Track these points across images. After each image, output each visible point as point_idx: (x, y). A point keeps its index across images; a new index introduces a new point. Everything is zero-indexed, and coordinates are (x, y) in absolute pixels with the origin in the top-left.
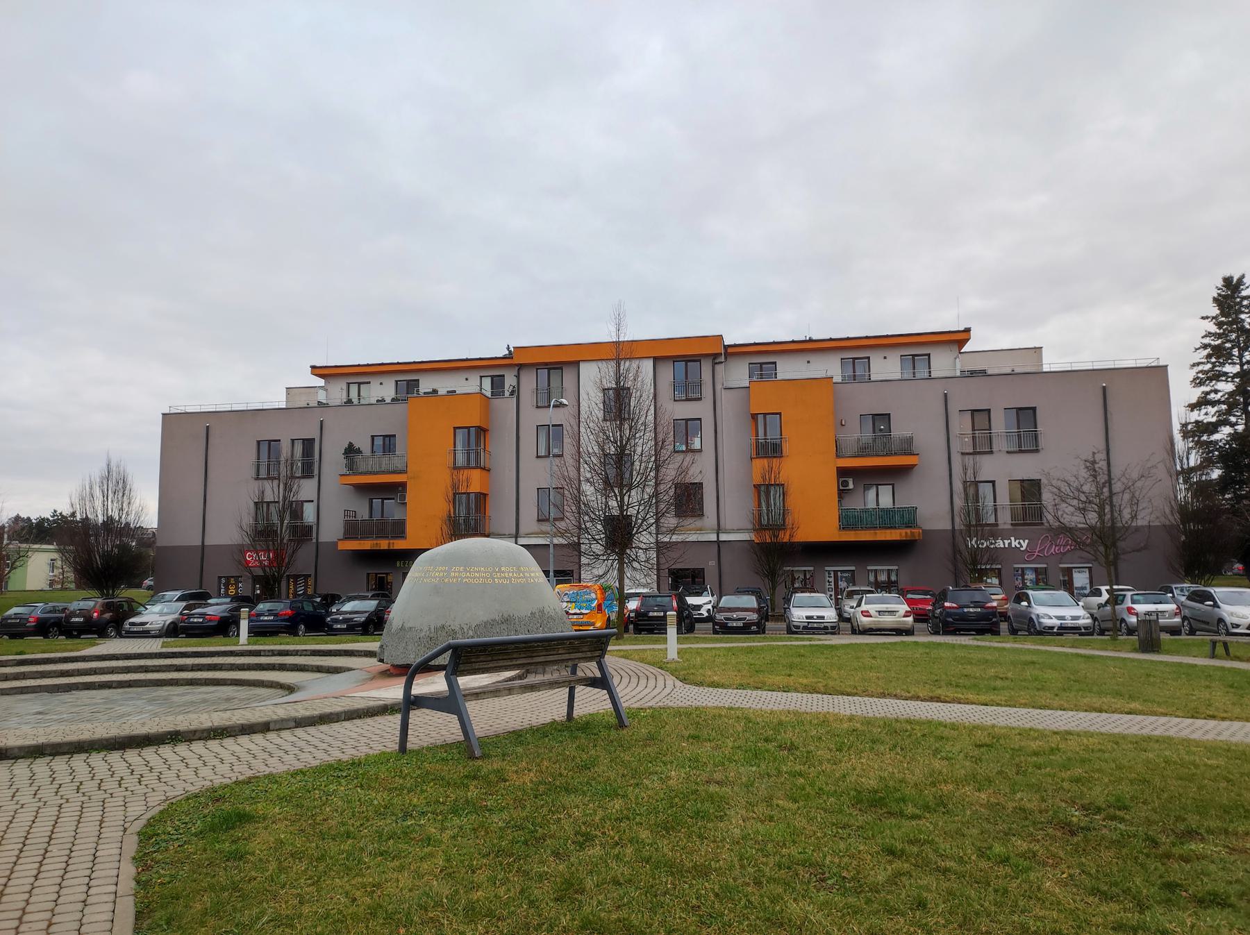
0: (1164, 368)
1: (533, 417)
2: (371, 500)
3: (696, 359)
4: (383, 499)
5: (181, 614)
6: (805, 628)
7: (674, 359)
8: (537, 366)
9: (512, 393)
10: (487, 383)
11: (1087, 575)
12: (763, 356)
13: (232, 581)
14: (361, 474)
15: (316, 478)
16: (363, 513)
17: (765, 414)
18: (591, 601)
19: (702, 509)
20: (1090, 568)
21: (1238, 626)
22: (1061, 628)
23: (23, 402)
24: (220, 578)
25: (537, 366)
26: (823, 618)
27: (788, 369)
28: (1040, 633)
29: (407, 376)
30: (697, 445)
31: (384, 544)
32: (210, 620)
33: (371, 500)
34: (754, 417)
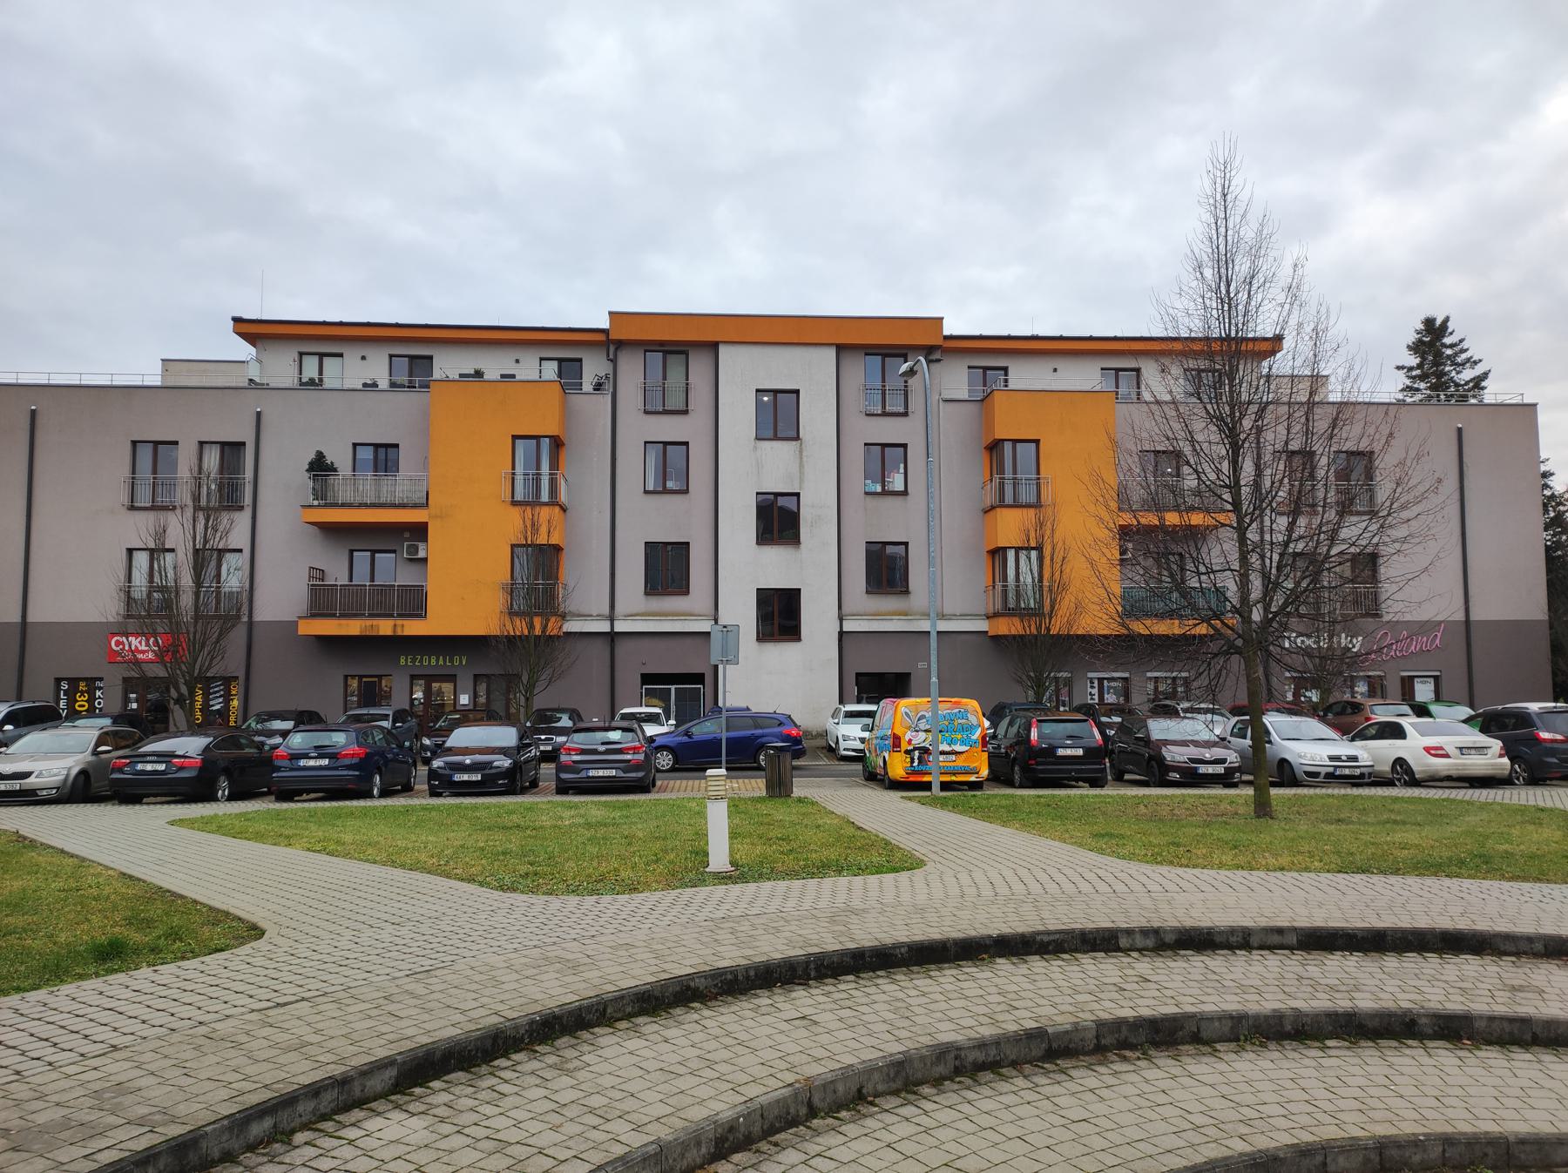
1: (639, 428)
2: (351, 552)
3: (902, 352)
4: (373, 552)
5: (95, 753)
6: (1329, 776)
7: (869, 350)
8: (648, 346)
9: (598, 387)
10: (550, 371)
11: (1431, 686)
12: (991, 355)
13: (82, 686)
14: (335, 505)
15: (247, 513)
16: (337, 575)
17: (1015, 441)
18: (971, 728)
20: (1436, 678)
24: (58, 681)
25: (648, 346)
26: (1355, 759)
27: (1025, 375)
30: (897, 482)
31: (385, 627)
32: (181, 768)
33: (351, 552)
34: (994, 447)
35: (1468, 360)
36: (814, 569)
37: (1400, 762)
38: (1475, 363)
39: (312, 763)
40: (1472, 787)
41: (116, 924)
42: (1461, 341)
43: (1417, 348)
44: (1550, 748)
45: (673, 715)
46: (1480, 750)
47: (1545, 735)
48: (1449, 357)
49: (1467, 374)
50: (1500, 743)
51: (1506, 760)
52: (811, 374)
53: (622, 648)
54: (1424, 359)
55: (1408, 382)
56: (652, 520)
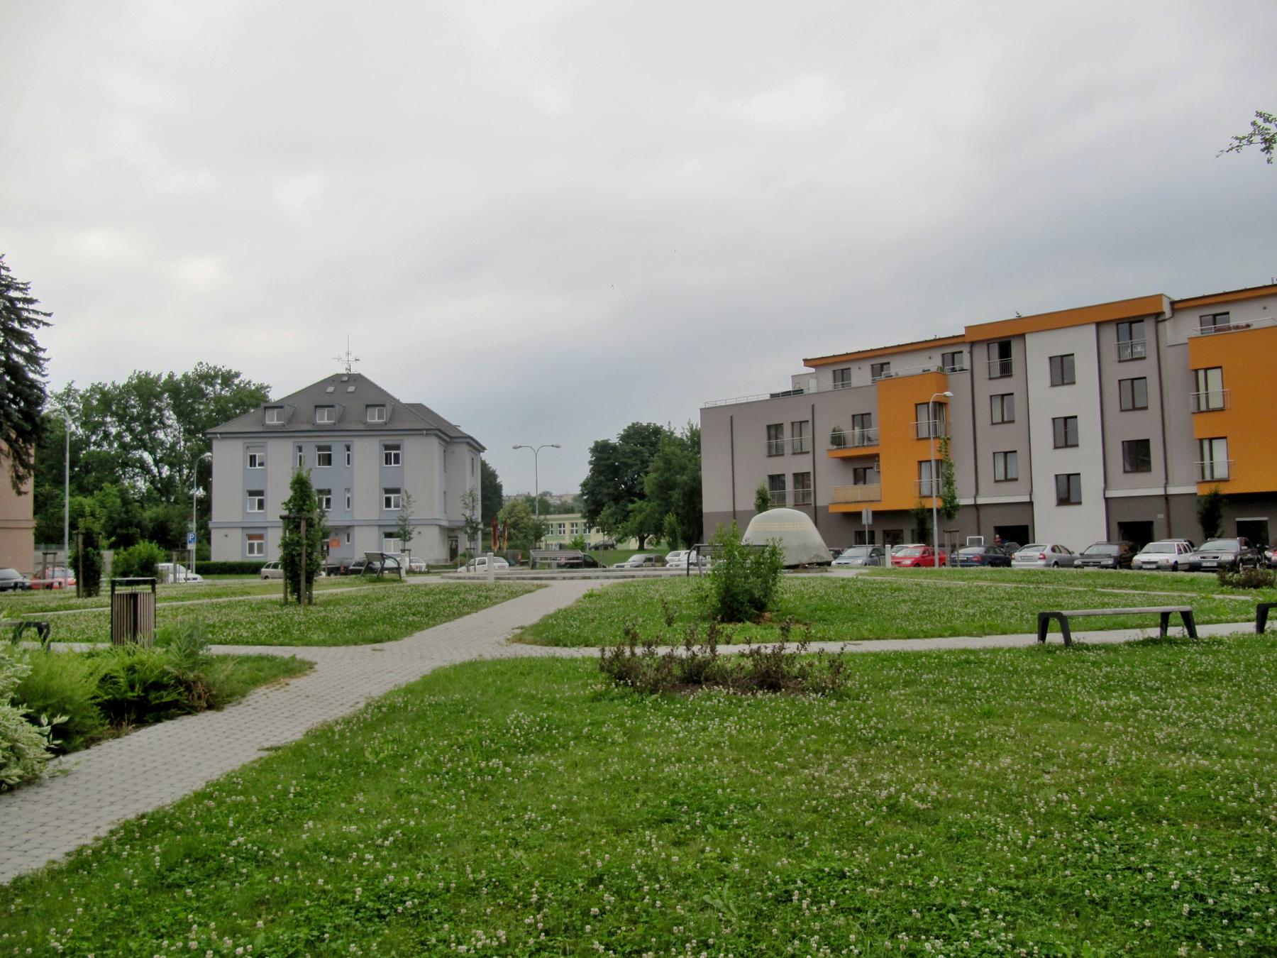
0: (1147, 441)
1: (987, 388)
12: (1213, 308)
19: (1149, 463)
23: (5, 880)
29: (879, 360)
36: (1086, 460)
41: (764, 901)
45: (303, 653)
52: (1081, 344)
53: (983, 512)
56: (994, 439)
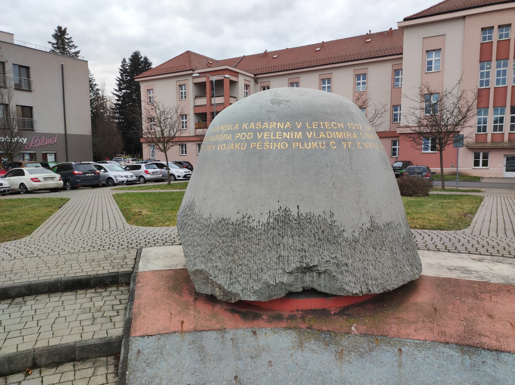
11: (53, 157)
20: (55, 154)
21: (180, 177)
22: (127, 181)
28: (115, 185)
35: (73, 45)
37: (22, 184)
38: (76, 47)
39: (90, 175)
40: (51, 192)
42: (71, 38)
43: (55, 36)
44: (78, 177)
46: (52, 178)
47: (76, 172)
48: (67, 43)
49: (73, 51)
50: (60, 176)
51: (62, 182)
54: (58, 41)
55: (53, 49)
